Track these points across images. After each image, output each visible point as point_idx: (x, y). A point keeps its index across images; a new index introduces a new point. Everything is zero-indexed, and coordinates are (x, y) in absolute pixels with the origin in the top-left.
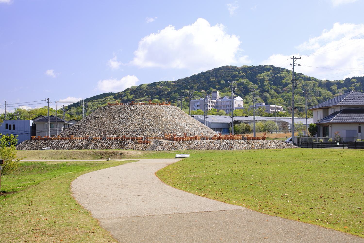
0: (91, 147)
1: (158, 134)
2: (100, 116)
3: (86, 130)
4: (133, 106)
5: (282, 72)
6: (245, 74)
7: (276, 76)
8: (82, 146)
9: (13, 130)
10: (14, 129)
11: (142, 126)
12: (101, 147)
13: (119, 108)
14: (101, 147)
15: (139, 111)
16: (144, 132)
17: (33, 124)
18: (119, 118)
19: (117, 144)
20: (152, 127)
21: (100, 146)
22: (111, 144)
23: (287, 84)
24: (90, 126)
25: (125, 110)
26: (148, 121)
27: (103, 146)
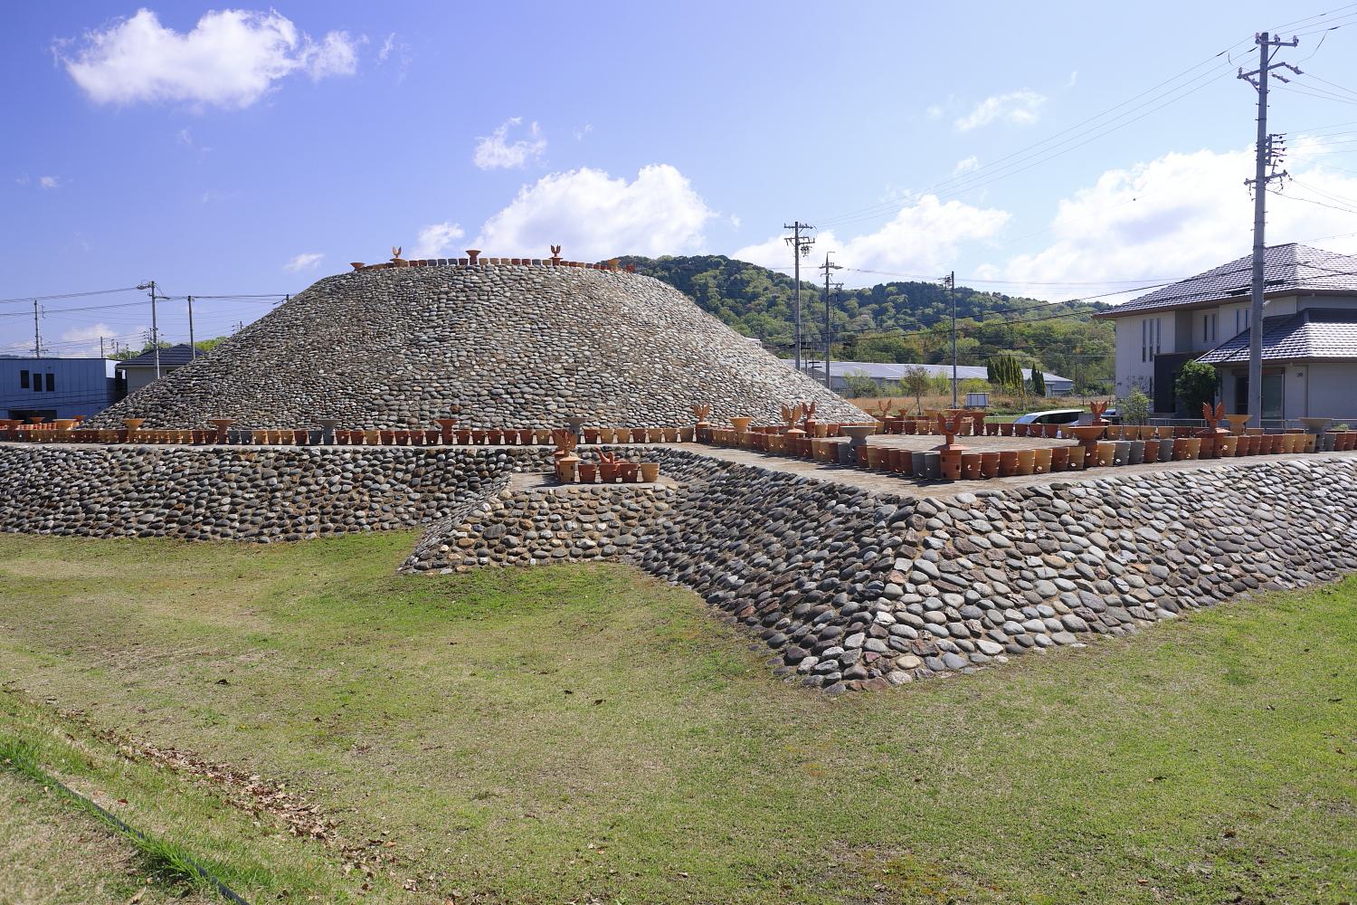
0: (233, 496)
1: (629, 406)
2: (311, 320)
3: (233, 390)
4: (477, 271)
5: (744, 271)
6: (667, 274)
7: (732, 278)
8: (173, 490)
9: (48, 390)
10: (51, 387)
11: (532, 366)
12: (298, 493)
13: (406, 280)
14: (298, 493)
15: (508, 294)
16: (547, 395)
17: (118, 374)
18: (410, 327)
19: (400, 475)
20: (590, 369)
21: (289, 489)
22: (364, 472)
23: (755, 296)
24: (255, 365)
25: (437, 287)
26: (560, 340)
27: (309, 491)
